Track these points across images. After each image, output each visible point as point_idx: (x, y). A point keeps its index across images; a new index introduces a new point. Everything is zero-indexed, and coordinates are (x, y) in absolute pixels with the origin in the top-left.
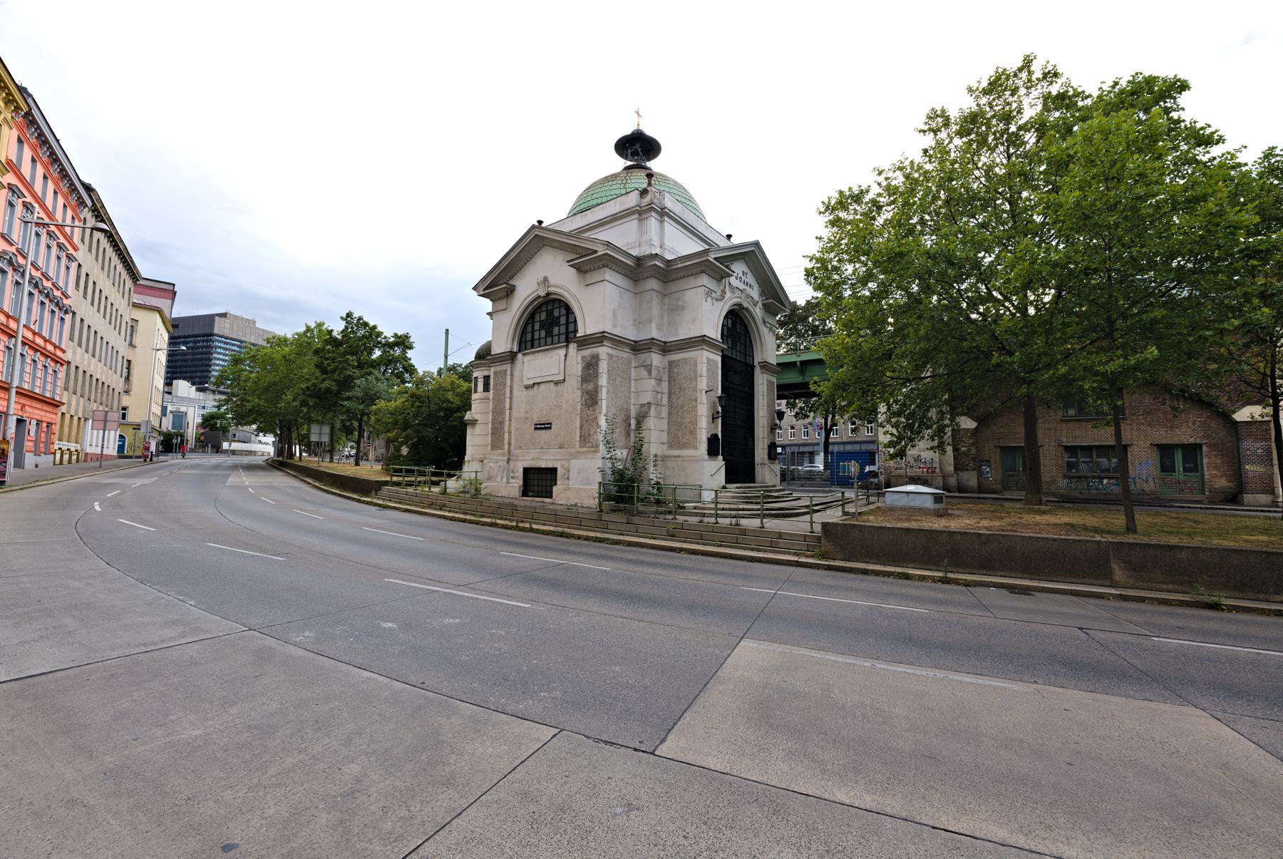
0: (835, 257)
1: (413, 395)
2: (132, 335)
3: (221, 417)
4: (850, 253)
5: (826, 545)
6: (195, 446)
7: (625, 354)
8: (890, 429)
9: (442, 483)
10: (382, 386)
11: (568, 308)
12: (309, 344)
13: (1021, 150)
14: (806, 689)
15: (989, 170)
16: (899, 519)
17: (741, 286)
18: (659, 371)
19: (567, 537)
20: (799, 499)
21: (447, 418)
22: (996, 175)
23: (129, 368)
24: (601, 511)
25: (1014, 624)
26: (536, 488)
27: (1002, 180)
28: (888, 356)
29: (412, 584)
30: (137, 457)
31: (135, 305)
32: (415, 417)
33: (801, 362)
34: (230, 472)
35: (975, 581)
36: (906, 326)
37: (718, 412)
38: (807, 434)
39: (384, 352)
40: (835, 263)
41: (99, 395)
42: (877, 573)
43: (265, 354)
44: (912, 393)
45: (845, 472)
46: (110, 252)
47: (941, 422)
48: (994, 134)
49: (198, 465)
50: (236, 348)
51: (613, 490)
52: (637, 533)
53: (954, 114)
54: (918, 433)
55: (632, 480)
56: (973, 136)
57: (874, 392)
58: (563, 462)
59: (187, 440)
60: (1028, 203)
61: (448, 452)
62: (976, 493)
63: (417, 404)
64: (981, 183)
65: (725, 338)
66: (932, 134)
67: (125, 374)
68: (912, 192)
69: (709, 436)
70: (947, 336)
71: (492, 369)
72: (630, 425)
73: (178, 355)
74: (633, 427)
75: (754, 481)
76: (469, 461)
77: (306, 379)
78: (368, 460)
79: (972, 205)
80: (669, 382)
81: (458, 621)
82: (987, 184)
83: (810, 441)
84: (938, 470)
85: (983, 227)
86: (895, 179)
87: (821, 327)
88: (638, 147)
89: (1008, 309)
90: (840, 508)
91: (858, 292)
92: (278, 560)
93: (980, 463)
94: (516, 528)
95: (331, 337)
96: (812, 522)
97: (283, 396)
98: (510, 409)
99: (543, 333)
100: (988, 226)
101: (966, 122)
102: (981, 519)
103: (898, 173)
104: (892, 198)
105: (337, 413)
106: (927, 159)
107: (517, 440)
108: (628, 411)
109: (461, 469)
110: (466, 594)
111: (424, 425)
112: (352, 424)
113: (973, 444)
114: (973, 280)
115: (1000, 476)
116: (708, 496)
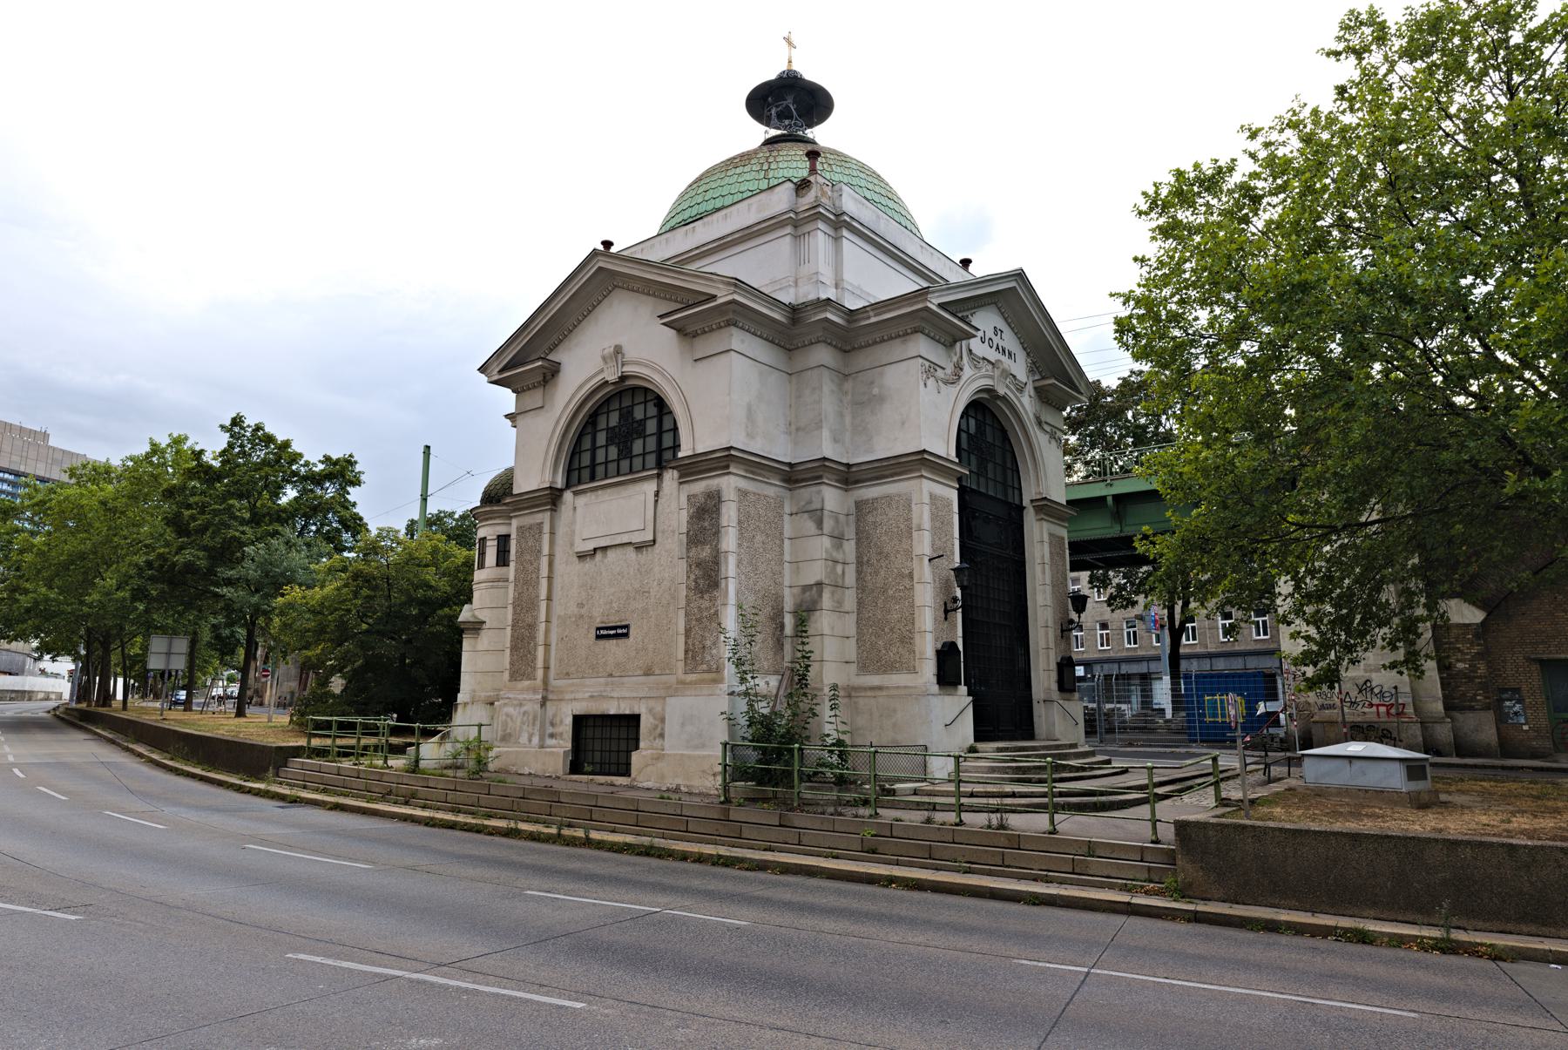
0: (1172, 296)
1: (356, 576)
5: (1187, 869)
7: (772, 489)
9: (411, 749)
10: (298, 558)
11: (661, 404)
12: (155, 477)
13: (1536, 77)
15: (1471, 119)
16: (1335, 814)
17: (993, 355)
18: (837, 521)
19: (659, 857)
20: (1125, 771)
21: (423, 618)
22: (1488, 127)
24: (727, 801)
26: (598, 755)
28: (1290, 481)
29: (345, 964)
32: (362, 617)
33: (1116, 497)
35: (1513, 949)
36: (1322, 423)
37: (955, 600)
38: (1134, 638)
39: (303, 492)
40: (1174, 307)
43: (67, 498)
44: (1343, 554)
45: (1215, 715)
47: (1408, 613)
48: (1479, 49)
51: (753, 756)
52: (800, 846)
53: (1394, 17)
54: (1363, 635)
55: (790, 737)
57: (1264, 553)
58: (652, 703)
60: (1556, 178)
61: (424, 686)
62: (1495, 757)
63: (365, 592)
64: (1457, 143)
65: (964, 455)
66: (1353, 59)
68: (1319, 167)
69: (939, 647)
70: (1407, 441)
71: (515, 523)
72: (782, 626)
77: (146, 546)
78: (261, 704)
79: (1441, 187)
80: (859, 542)
81: (436, 1041)
83: (1141, 653)
84: (1410, 710)
85: (1467, 228)
86: (1284, 144)
87: (1151, 429)
88: (789, 102)
89: (1531, 384)
90: (1211, 790)
92: (68, 921)
93: (1497, 695)
94: (557, 839)
95: (200, 465)
96: (1154, 822)
97: (97, 581)
98: (549, 599)
99: (613, 452)
100: (1477, 226)
101: (1420, 31)
102: (1513, 814)
103: (1289, 133)
104: (1279, 181)
106: (1345, 105)
107: (561, 660)
108: (779, 599)
111: (378, 632)
112: (233, 634)
114: (1452, 330)
116: (941, 768)
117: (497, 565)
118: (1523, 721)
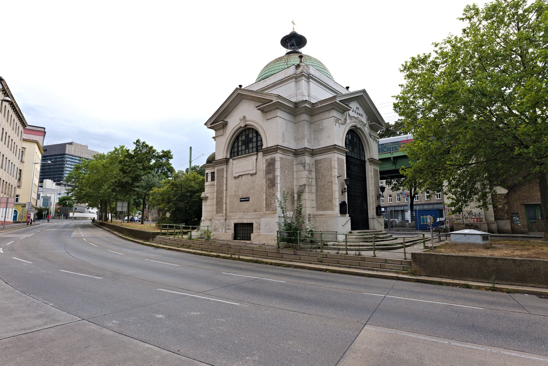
0: (411, 96)
1: (173, 184)
2: (22, 156)
3: (69, 199)
4: (420, 93)
5: (415, 267)
6: (55, 215)
7: (290, 157)
8: (451, 195)
10: (156, 180)
11: (257, 133)
12: (116, 158)
13: (527, 24)
14: (407, 357)
15: (506, 38)
16: (460, 251)
17: (356, 116)
18: (309, 166)
19: (260, 263)
20: (396, 239)
21: (191, 196)
22: (511, 40)
23: (20, 174)
24: (279, 247)
25: (544, 319)
26: (241, 235)
27: (514, 43)
28: (448, 152)
30: (23, 222)
31: (25, 140)
32: (174, 196)
33: (394, 158)
34: (73, 229)
35: (514, 290)
36: (458, 133)
37: (345, 189)
39: (157, 161)
40: (412, 99)
41: (4, 189)
42: (448, 284)
43: (93, 164)
46: (12, 112)
49: (56, 226)
50: (77, 161)
51: (285, 235)
52: (300, 260)
53: (481, 7)
54: (470, 197)
55: (296, 229)
56: (494, 19)
58: (256, 220)
59: (51, 212)
61: (192, 215)
62: (510, 234)
63: (175, 189)
64: (501, 46)
65: (347, 146)
67: (18, 177)
68: (457, 55)
69: (340, 203)
70: (484, 138)
71: (216, 168)
72: (294, 197)
73: (46, 166)
74: (296, 198)
75: (368, 229)
76: (204, 220)
77: (115, 177)
78: (148, 221)
81: (198, 313)
82: (505, 46)
84: (484, 220)
85: (504, 72)
86: (446, 48)
88: (294, 41)
91: (426, 115)
95: (128, 154)
96: (405, 253)
97: (102, 187)
99: (244, 147)
100: (507, 71)
101: (489, 11)
102: (515, 250)
103: (448, 44)
104: (444, 60)
105: (132, 195)
106: (466, 35)
109: (200, 225)
110: (202, 297)
111: (179, 200)
112: (139, 201)
113: (506, 203)
114: (499, 104)
115: (525, 223)
116: (341, 238)
117: (211, 181)
118: (519, 223)
